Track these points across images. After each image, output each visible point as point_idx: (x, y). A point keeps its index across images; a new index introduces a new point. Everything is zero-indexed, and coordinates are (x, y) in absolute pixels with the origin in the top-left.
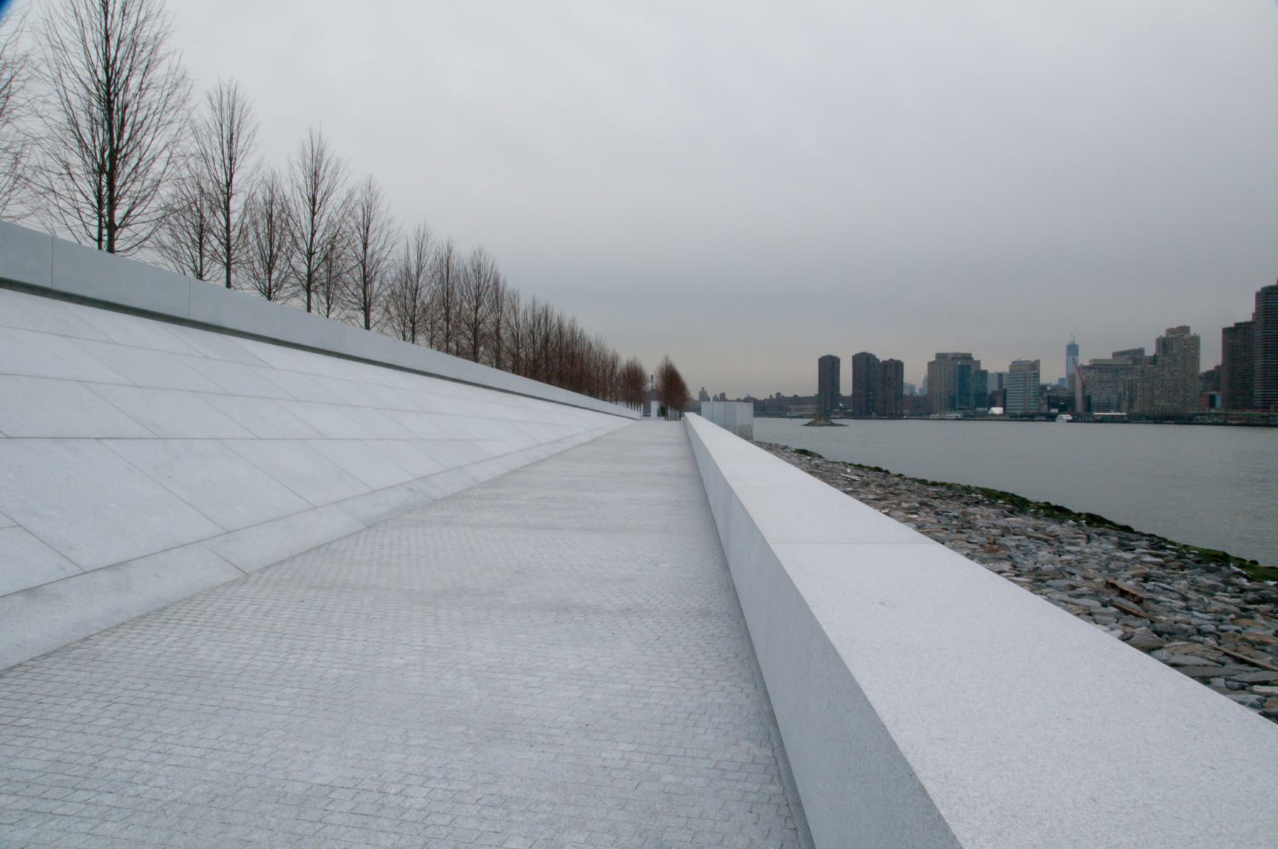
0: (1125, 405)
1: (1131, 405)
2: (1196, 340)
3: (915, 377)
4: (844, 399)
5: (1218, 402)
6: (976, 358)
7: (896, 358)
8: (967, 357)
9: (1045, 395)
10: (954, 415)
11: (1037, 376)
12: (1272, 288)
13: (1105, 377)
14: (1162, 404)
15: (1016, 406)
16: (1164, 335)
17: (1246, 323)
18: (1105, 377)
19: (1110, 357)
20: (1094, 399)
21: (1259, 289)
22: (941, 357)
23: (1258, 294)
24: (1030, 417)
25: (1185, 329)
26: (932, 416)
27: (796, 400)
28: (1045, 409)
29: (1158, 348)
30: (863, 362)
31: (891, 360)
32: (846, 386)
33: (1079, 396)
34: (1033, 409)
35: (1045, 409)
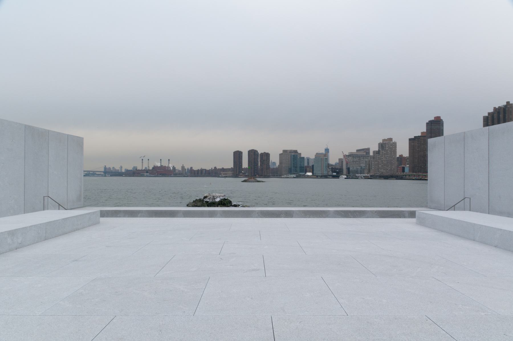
0: (366, 171)
1: (369, 172)
2: (395, 144)
3: (275, 159)
4: (243, 169)
5: (407, 170)
6: (299, 152)
7: (267, 152)
8: (296, 152)
9: (330, 167)
10: (293, 176)
11: (327, 159)
12: (432, 121)
13: (355, 160)
14: (383, 171)
15: (318, 172)
16: (381, 142)
17: (419, 136)
18: (355, 160)
19: (355, 151)
20: (351, 169)
21: (442, 118)
22: (285, 151)
23: (427, 124)
24: (326, 177)
25: (391, 139)
26: (283, 176)
27: (223, 170)
28: (330, 173)
29: (379, 147)
30: (253, 153)
31: (265, 153)
32: (245, 164)
33: (344, 167)
34: (325, 173)
35: (330, 173)
